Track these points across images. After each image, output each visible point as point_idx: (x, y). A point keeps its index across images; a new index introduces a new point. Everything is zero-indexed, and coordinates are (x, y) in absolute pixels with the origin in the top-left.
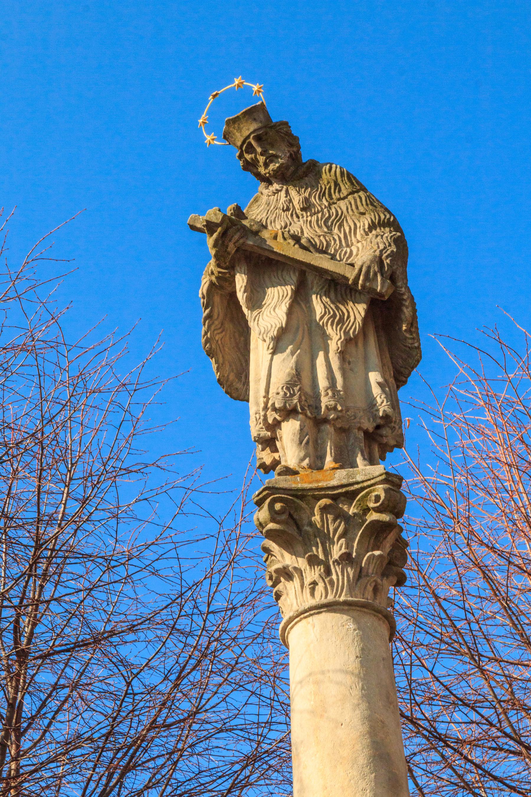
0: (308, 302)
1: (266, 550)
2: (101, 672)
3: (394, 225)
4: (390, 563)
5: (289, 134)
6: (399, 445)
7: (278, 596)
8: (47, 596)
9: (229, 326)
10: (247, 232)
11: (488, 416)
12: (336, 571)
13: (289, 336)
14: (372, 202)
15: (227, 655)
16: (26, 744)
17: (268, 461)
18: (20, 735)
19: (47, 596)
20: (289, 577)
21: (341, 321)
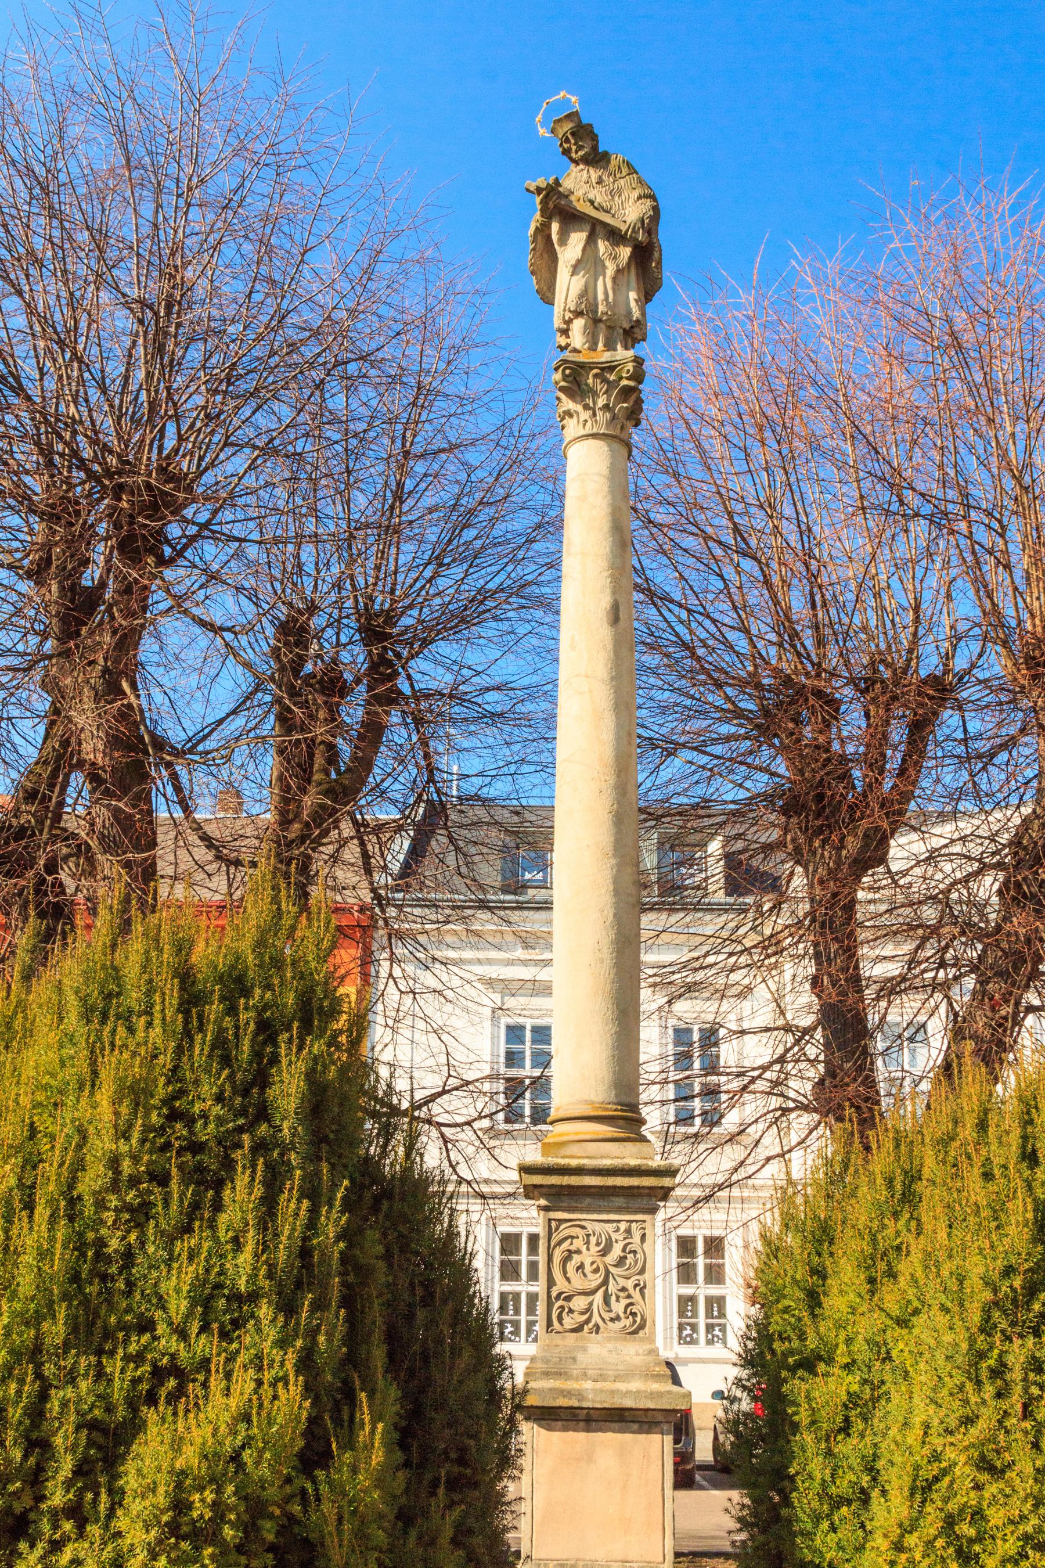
0: (596, 243)
1: (558, 399)
2: (452, 468)
3: (653, 197)
4: (632, 412)
5: (592, 132)
6: (644, 340)
7: (563, 428)
8: (423, 418)
9: (545, 256)
10: (562, 196)
11: (698, 327)
12: (599, 414)
13: (582, 265)
14: (640, 181)
15: (527, 464)
16: (405, 508)
17: (563, 344)
18: (402, 503)
19: (423, 418)
20: (571, 416)
21: (615, 258)
